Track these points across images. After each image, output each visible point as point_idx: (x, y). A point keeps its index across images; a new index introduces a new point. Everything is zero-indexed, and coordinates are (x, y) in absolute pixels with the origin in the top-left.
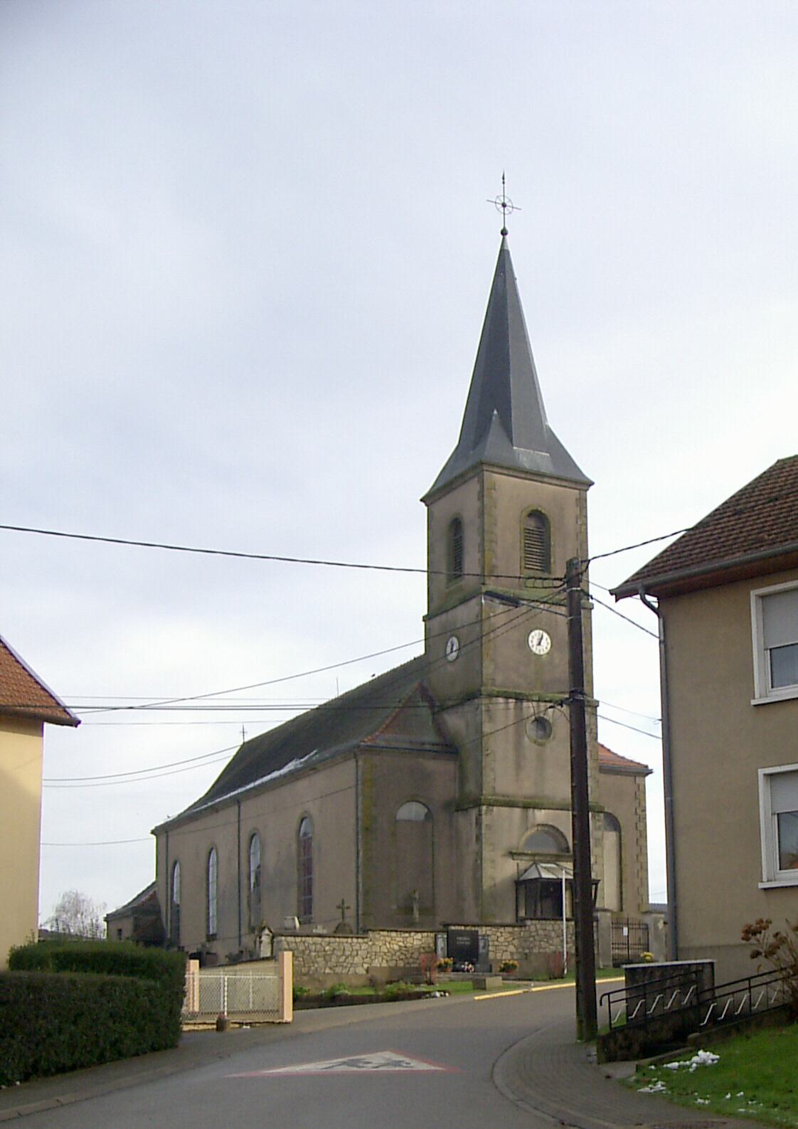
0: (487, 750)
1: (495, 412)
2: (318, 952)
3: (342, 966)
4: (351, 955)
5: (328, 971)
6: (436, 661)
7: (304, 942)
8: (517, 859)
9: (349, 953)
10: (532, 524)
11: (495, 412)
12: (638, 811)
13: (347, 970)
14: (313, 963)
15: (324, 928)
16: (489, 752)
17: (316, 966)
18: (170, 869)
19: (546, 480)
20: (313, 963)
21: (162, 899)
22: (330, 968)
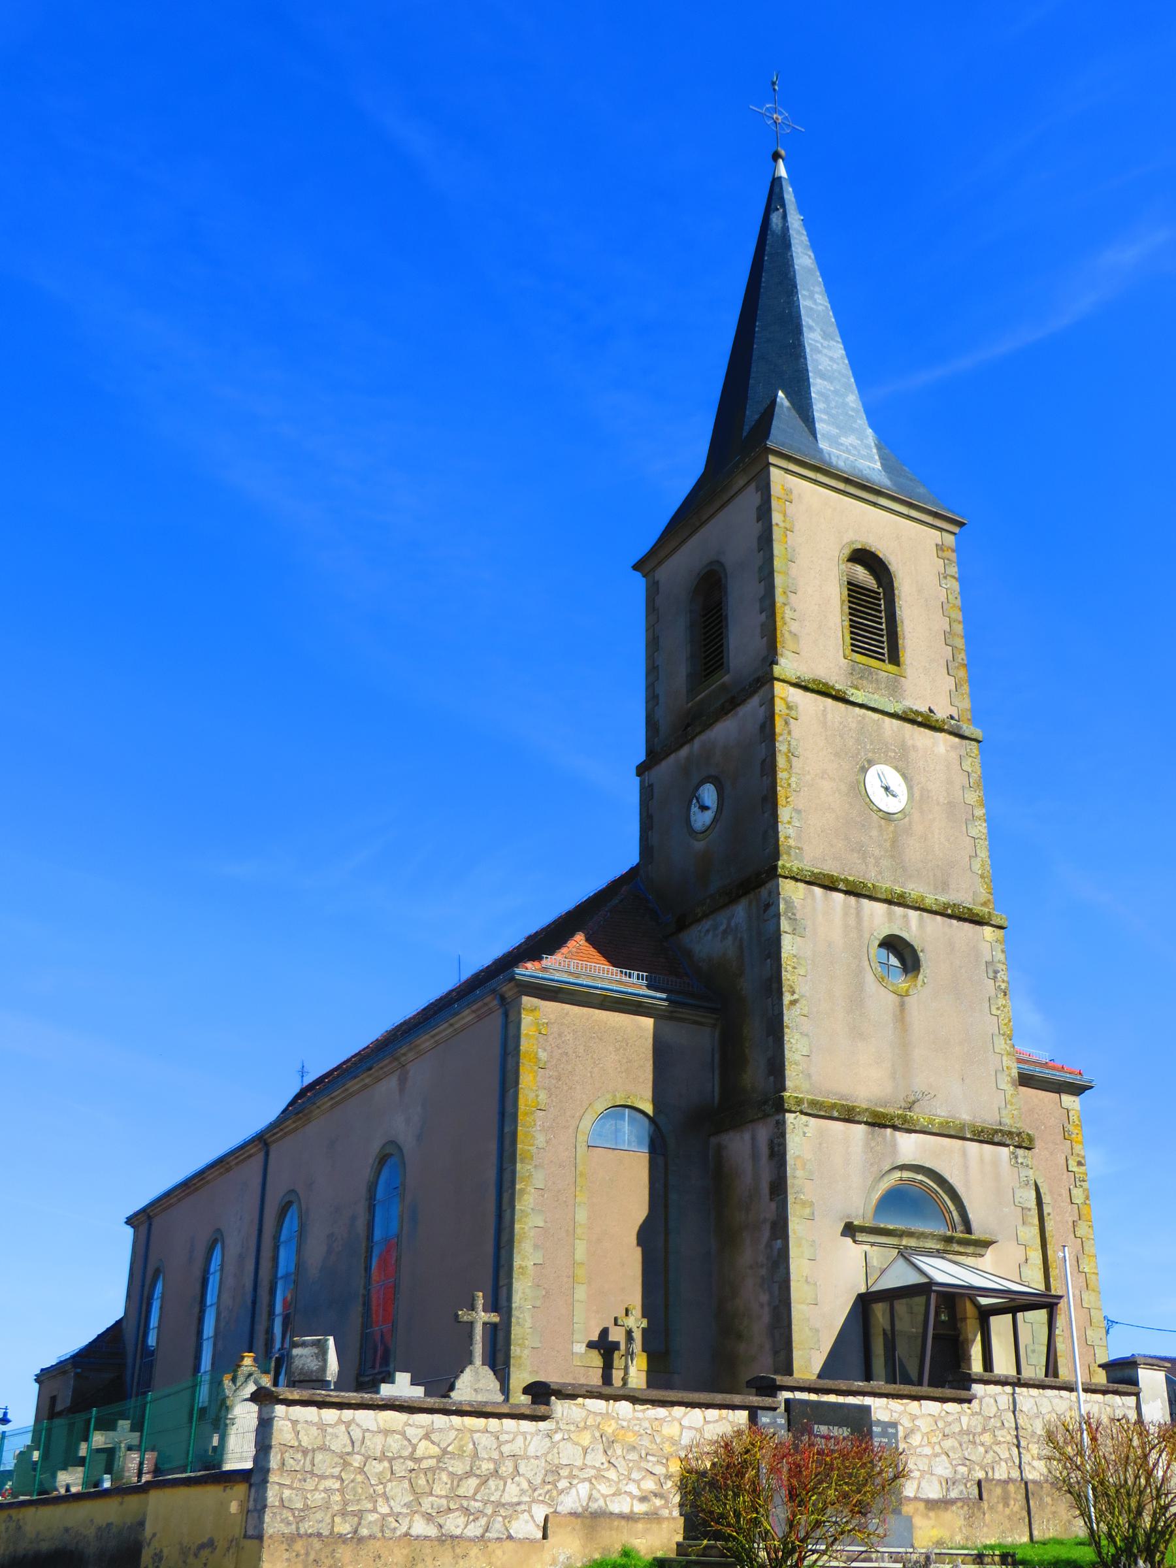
0: (793, 993)
1: (780, 394)
2: (391, 1460)
3: (466, 1511)
4: (496, 1473)
5: (420, 1527)
6: (377, 1423)
7: (348, 1424)
8: (862, 1243)
9: (491, 1466)
10: (862, 574)
11: (780, 394)
12: (1070, 1162)
13: (483, 1521)
14: (373, 1499)
15: (414, 1383)
16: (796, 996)
17: (384, 1509)
18: (148, 1282)
19: (883, 501)
20: (373, 1499)
21: (129, 1332)
22: (429, 1518)
